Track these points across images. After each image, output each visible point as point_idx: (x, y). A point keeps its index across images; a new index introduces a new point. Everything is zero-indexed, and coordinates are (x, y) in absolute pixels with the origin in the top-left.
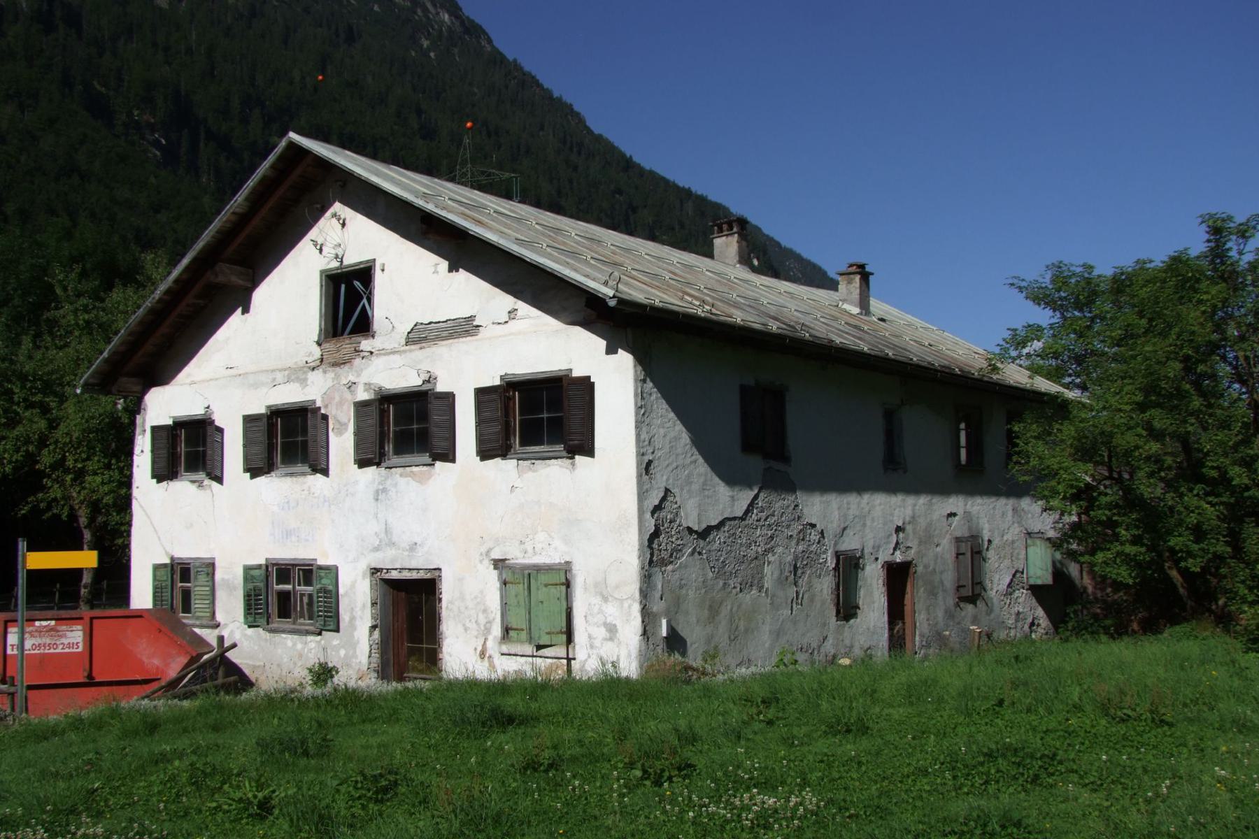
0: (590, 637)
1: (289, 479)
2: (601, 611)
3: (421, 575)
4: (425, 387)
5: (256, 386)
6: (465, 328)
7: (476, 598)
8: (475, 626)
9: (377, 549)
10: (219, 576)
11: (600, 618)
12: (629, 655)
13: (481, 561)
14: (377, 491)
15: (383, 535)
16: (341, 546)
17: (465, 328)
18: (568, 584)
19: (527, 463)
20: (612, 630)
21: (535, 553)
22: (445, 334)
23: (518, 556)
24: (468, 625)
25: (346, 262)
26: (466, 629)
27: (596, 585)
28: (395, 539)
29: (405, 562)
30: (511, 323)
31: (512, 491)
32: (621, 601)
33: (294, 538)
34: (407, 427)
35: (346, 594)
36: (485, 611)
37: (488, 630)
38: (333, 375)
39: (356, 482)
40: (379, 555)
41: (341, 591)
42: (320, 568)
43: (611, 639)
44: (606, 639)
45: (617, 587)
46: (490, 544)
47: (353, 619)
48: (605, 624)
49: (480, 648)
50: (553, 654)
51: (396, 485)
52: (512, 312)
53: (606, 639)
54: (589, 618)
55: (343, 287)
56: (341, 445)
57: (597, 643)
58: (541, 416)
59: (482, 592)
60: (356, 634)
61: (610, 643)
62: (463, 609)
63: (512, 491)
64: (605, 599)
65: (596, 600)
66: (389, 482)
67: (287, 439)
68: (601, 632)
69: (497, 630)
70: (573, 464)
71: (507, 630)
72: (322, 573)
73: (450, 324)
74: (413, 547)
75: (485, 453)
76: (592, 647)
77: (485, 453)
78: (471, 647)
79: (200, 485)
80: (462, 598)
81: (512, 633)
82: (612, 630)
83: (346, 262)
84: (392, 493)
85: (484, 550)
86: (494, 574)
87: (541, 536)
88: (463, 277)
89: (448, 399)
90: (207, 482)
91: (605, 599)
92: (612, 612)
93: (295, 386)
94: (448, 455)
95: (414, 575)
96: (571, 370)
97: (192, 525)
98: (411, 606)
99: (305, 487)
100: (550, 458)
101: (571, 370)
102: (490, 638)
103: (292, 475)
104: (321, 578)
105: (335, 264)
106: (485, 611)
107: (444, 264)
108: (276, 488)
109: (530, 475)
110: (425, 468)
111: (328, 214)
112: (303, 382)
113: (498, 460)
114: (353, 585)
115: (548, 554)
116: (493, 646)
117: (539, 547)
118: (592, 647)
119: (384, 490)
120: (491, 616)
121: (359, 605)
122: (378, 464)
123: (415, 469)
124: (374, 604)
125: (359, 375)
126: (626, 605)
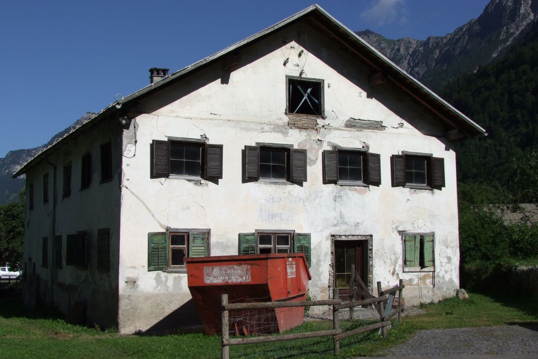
0: (441, 262)
1: (273, 186)
2: (445, 252)
3: (360, 238)
4: (363, 150)
5: (247, 129)
6: (378, 126)
7: (390, 248)
8: (389, 261)
9: (336, 225)
10: (213, 240)
11: (445, 255)
12: (455, 268)
13: (393, 232)
14: (335, 197)
15: (339, 219)
16: (312, 223)
17: (378, 126)
18: (433, 241)
19: (413, 190)
20: (449, 259)
21: (418, 228)
22: (365, 126)
23: (411, 229)
24: (386, 260)
25: (304, 76)
26: (385, 263)
27: (443, 241)
28: (346, 221)
29: (348, 231)
30: (400, 129)
31: (407, 202)
32: (453, 247)
33: (277, 218)
34: (352, 167)
35: (314, 248)
36: (395, 254)
37: (396, 262)
38: (306, 134)
39: (322, 191)
40: (337, 228)
41: (312, 247)
42: (300, 235)
43: (449, 263)
44: (447, 263)
45: (451, 242)
46: (397, 224)
47: (319, 261)
48: (447, 257)
49: (392, 271)
50: (428, 270)
51: (347, 194)
52: (402, 125)
53: (447, 263)
54: (441, 255)
55: (299, 87)
56: (315, 170)
57: (443, 264)
58: (416, 171)
59: (393, 245)
60: (321, 269)
61: (448, 265)
62: (383, 253)
63: (407, 202)
64: (447, 247)
65: (444, 247)
66: (342, 193)
67: (272, 163)
68: (445, 260)
69: (400, 262)
70: (433, 193)
71: (405, 262)
72: (301, 238)
73: (369, 122)
74: (357, 225)
75: (395, 183)
76: (442, 266)
77: (395, 183)
78: (384, 272)
79: (197, 183)
80: (383, 248)
81: (407, 263)
82: (449, 259)
83: (304, 76)
84: (344, 198)
85: (394, 227)
86: (399, 237)
87: (421, 221)
88: (374, 102)
89: (377, 157)
90: (203, 181)
91: (447, 247)
92: (449, 252)
93: (280, 135)
94: (377, 183)
95: (355, 238)
96: (432, 154)
97: (188, 208)
98: (352, 255)
99: (287, 191)
100: (422, 189)
101: (432, 154)
102: (397, 265)
103: (275, 183)
104: (300, 240)
105: (297, 74)
106: (395, 254)
107: (364, 94)
108: (265, 190)
109: (415, 195)
110: (363, 188)
111: (302, 48)
112: (285, 134)
113: (401, 187)
114: (319, 244)
115: (423, 229)
116: (399, 269)
117: (420, 225)
118: (442, 266)
119: (340, 196)
120: (398, 256)
121: (323, 253)
122: (335, 183)
123: (356, 187)
124: (332, 253)
125: (324, 137)
126: (454, 249)
